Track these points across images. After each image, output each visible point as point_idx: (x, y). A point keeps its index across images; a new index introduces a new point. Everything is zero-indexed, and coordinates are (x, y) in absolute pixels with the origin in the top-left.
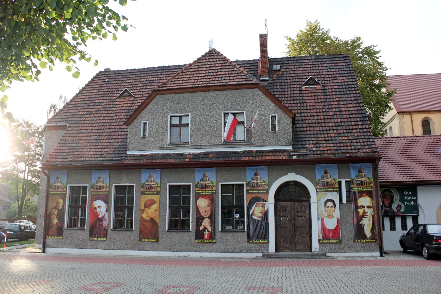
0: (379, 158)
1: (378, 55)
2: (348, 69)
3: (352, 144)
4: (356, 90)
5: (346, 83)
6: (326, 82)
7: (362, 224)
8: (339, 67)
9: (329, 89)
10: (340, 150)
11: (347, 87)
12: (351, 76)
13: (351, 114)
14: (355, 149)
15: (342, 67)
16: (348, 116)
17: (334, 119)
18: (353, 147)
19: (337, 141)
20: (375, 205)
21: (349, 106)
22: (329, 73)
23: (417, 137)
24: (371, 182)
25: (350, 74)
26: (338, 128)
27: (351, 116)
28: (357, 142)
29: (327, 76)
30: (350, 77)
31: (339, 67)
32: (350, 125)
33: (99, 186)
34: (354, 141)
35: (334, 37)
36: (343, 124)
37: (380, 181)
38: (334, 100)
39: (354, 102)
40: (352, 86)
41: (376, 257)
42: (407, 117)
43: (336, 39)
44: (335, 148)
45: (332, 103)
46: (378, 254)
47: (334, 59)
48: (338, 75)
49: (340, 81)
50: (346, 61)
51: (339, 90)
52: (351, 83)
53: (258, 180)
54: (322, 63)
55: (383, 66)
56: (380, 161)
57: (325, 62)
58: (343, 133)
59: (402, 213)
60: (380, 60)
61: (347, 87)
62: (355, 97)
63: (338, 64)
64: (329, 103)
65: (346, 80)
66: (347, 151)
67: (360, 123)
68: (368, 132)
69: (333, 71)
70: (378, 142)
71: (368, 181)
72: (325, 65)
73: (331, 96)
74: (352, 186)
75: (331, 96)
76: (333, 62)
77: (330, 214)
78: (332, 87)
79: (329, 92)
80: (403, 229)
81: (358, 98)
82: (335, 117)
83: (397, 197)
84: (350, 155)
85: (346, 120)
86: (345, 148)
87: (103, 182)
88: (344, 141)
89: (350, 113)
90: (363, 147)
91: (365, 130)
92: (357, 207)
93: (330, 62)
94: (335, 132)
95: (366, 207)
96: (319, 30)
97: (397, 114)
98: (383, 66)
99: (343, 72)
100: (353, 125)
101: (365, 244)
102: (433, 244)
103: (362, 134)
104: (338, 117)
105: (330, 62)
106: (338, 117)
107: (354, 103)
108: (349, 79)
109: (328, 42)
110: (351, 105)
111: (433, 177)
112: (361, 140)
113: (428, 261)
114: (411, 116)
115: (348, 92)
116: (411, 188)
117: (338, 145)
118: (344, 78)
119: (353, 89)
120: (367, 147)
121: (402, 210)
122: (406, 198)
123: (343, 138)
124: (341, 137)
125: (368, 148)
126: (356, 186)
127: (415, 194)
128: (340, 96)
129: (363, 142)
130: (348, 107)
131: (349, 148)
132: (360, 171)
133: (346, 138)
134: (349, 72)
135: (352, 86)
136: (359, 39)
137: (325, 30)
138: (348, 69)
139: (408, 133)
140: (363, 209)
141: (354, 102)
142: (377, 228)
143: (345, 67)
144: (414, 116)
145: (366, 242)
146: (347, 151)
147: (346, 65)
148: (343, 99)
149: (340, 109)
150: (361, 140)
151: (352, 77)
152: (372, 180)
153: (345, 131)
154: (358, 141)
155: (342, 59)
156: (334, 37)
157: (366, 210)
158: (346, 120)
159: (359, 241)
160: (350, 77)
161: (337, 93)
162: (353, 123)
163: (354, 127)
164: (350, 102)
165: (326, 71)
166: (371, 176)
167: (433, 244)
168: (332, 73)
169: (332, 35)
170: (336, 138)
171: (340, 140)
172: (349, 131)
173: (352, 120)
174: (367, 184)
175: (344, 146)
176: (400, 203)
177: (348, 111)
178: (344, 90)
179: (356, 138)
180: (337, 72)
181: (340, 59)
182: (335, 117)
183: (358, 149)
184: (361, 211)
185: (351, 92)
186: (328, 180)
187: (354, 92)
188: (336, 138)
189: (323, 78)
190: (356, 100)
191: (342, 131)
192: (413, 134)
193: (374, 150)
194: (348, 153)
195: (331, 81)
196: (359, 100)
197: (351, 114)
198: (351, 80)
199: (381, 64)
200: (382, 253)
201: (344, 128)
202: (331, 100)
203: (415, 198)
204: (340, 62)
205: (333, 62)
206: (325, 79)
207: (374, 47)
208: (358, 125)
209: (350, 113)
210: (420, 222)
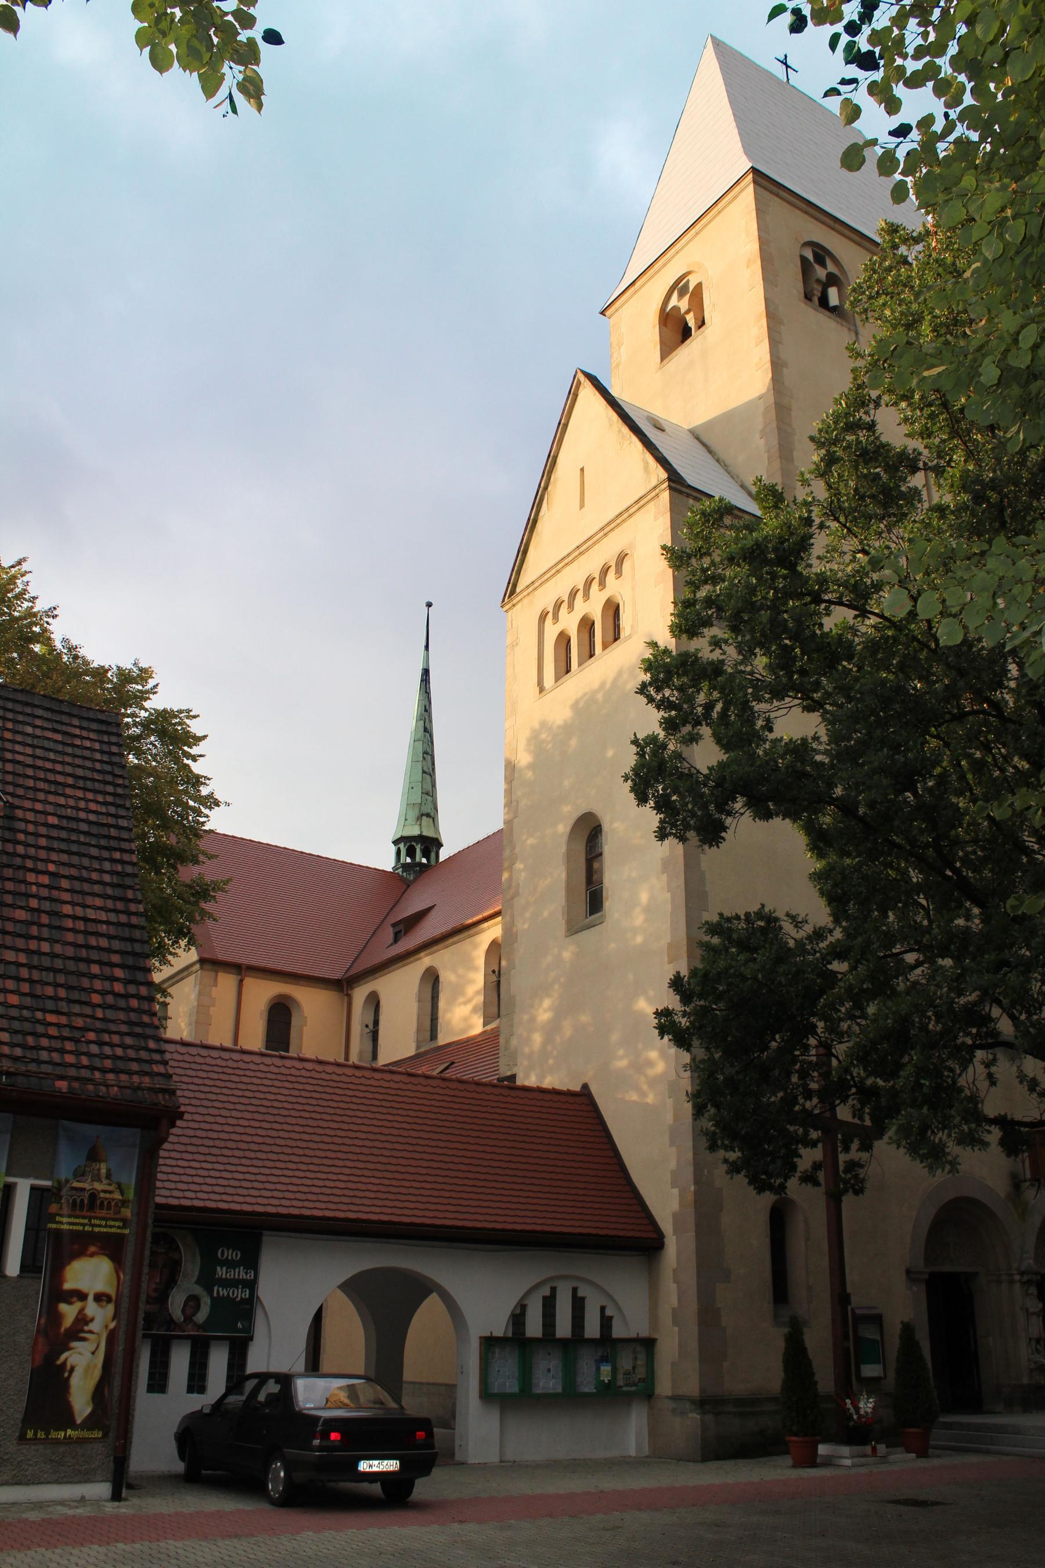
0: (174, 1115)
1: (194, 751)
2: (108, 768)
3: (83, 1048)
4: (123, 851)
5: (92, 817)
6: (20, 792)
7: (65, 1363)
8: (79, 752)
9: (27, 822)
10: (33, 1060)
11: (94, 830)
12: (114, 795)
13: (93, 934)
14: (92, 1068)
15: (87, 753)
16: (80, 939)
17: (28, 937)
18: (85, 1061)
19: (27, 1026)
20: (126, 1291)
21: (89, 900)
22: (40, 763)
23: (243, 1052)
24: (124, 1203)
25: (110, 789)
26: (36, 975)
27: (93, 941)
28: (101, 1044)
29: (30, 772)
30: (110, 799)
31: (79, 752)
32: (83, 975)
33: (87, 1195)
34: (92, 1036)
35: (65, 640)
36: (59, 964)
37: (158, 1200)
38: (41, 866)
39: (109, 891)
40: (113, 832)
41: (97, 1502)
42: (227, 982)
43: (70, 649)
44: (18, 1052)
45: (31, 877)
46: (102, 1489)
47: (64, 719)
48: (70, 781)
49: (71, 802)
50: (106, 738)
51: (64, 834)
52: (111, 821)
54: (20, 718)
55: (204, 791)
56: (174, 1125)
57: (29, 720)
58: (56, 999)
59: (200, 1327)
60: (197, 768)
61: (94, 830)
62: (118, 873)
63: (78, 742)
64: (20, 874)
65: (93, 806)
66: (59, 1071)
67: (119, 973)
68: (145, 1012)
69: (54, 761)
70: (176, 1056)
71: (117, 1196)
72: (29, 730)
73: (32, 851)
74: (54, 1208)
75: (32, 851)
76: (58, 727)
78: (41, 818)
79: (27, 833)
80: (191, 1389)
81: (128, 881)
82: (34, 931)
83: (191, 1267)
84: (70, 1087)
85: (70, 951)
86: (56, 1057)
88: (53, 1031)
89: (92, 928)
90: (121, 1065)
91: (134, 1003)
92: (58, 1295)
93: (46, 725)
94: (25, 988)
95: (91, 1298)
96: (20, 596)
97: (198, 966)
98: (204, 791)
99: (88, 774)
100: (95, 976)
101: (62, 1449)
102: (312, 1449)
103: (122, 1016)
104: (46, 933)
105: (46, 725)
106: (46, 933)
107: (109, 897)
108: (105, 804)
109: (37, 648)
110: (99, 902)
111: (373, 1209)
112: (116, 1039)
113: (283, 1510)
114: (241, 981)
115: (94, 852)
116: (240, 1236)
117: (30, 1041)
118: (90, 796)
119: (113, 843)
120: (135, 1066)
121: (201, 1316)
122: (221, 1272)
123: (51, 1018)
124: (44, 1011)
125: (136, 1073)
126: (65, 1211)
127: (252, 1261)
128: (64, 858)
129: (125, 1047)
130: (85, 906)
131: (70, 1059)
132: (93, 1156)
133: (64, 1020)
134: (109, 778)
135: (113, 832)
136: (144, 674)
137: (40, 606)
138: (108, 768)
139: (220, 1035)
140: (78, 1305)
141: (109, 891)
142: (117, 1382)
143: (98, 756)
144: (249, 982)
145: (68, 1440)
146: (59, 1071)
147: (102, 752)
148: (74, 872)
149: (56, 907)
150: (116, 1039)
151: (119, 801)
152: (131, 1194)
153: (62, 993)
154: (106, 1038)
155: (94, 726)
156: (65, 640)
157: (91, 1308)
158: (70, 951)
159: (41, 1435)
160: (110, 799)
161: (56, 845)
162: (95, 969)
163: (98, 985)
164: (97, 888)
165: (29, 751)
166: (130, 1179)
167: (312, 1449)
168: (49, 765)
169: (59, 631)
170: (26, 1013)
171: (38, 1021)
172: (76, 995)
173: (94, 955)
174: (109, 1208)
175: (50, 1050)
176: (198, 1290)
177: (86, 920)
178: (82, 838)
179: (99, 1025)
180: (69, 769)
181: (85, 724)
182: (34, 931)
183: (104, 1071)
184: (69, 1312)
185: (106, 854)
186: (98, 1186)
187: (117, 855)
188: (26, 1013)
189: (13, 773)
190: (118, 886)
191: (50, 991)
192: (236, 1041)
193: (160, 1083)
194: (62, 1078)
195: (41, 796)
196: (130, 887)
197: (93, 934)
198: (112, 810)
199: (197, 781)
200: (122, 1484)
201: (61, 979)
202: (29, 864)
203: (251, 1275)
204: (85, 734)
205: (58, 727)
206: (21, 781)
207: (188, 717)
208: (113, 979)
209: (92, 928)
210: (250, 1369)
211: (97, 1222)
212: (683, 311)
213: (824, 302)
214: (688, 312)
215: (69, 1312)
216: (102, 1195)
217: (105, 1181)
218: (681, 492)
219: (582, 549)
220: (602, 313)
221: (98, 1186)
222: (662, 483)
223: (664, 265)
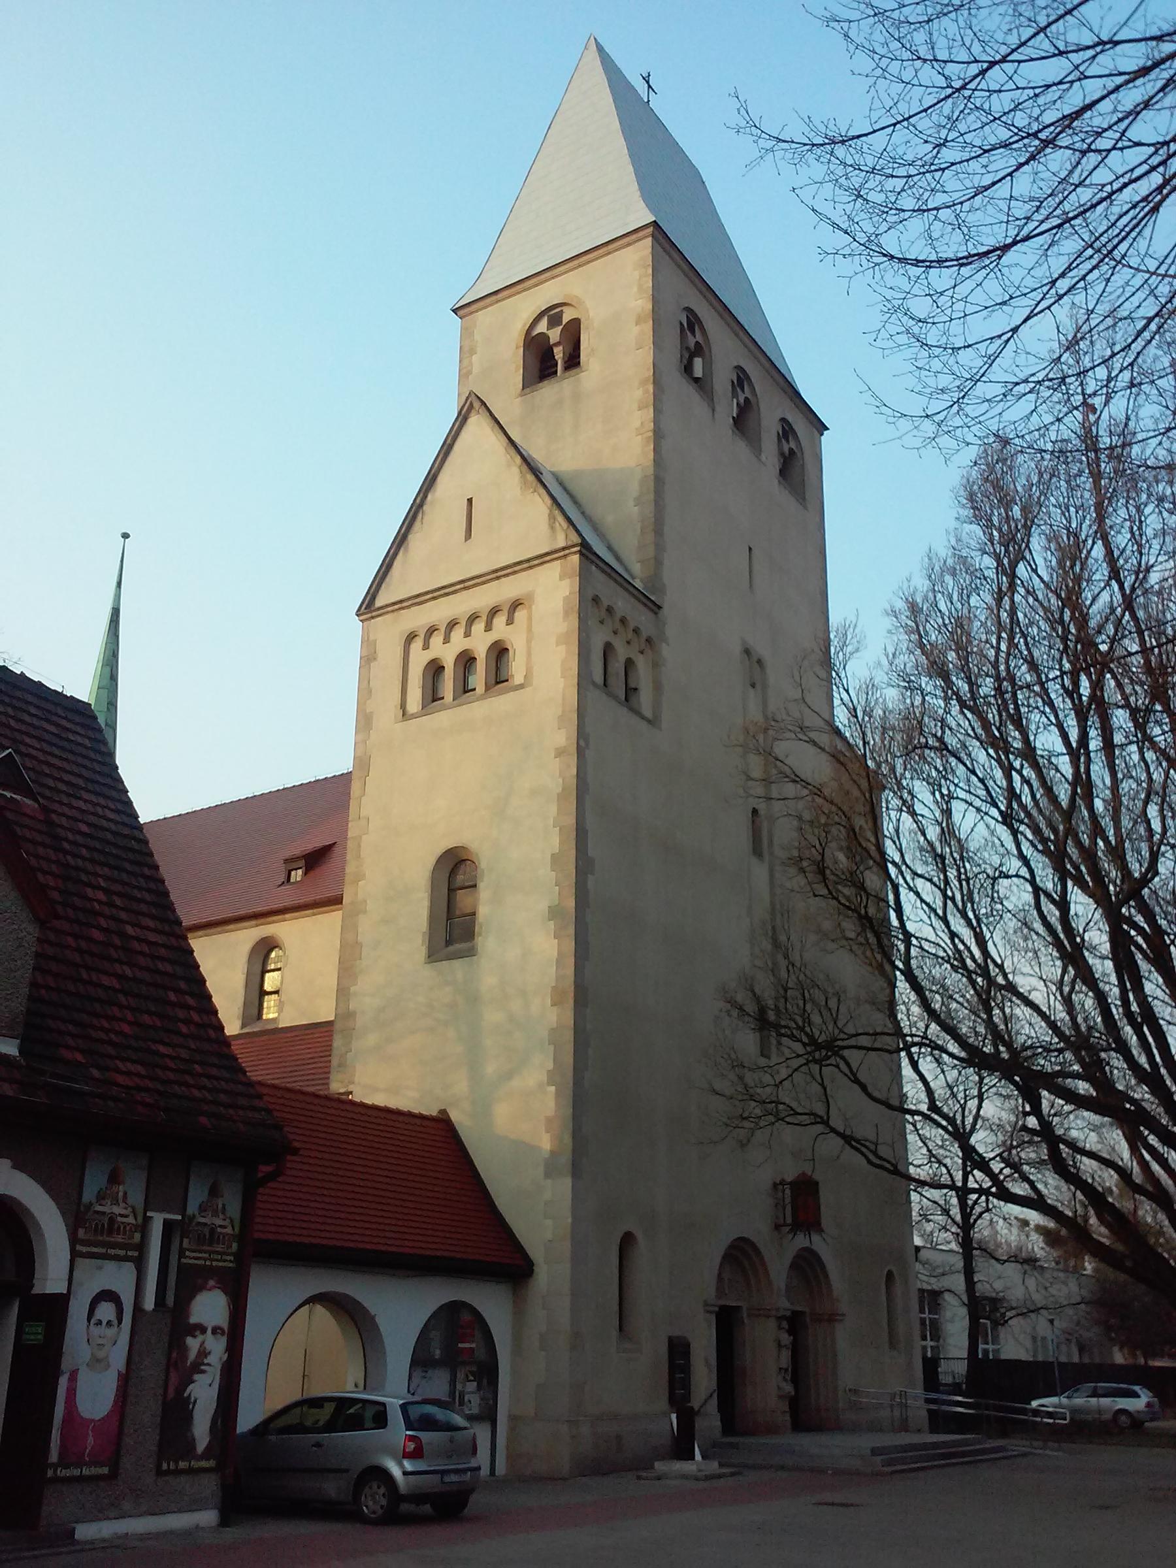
37: (256, 1235)
46: (208, 1517)
53: (215, 1214)
77: (101, 1354)
87: (124, 1201)
95: (209, 1331)
145: (191, 1471)
184: (193, 1344)
211: (216, 1257)
212: (552, 342)
213: (688, 369)
214: (557, 344)
215: (193, 1344)
216: (219, 1230)
217: (122, 1205)
218: (587, 558)
219: (467, 584)
220: (455, 311)
221: (117, 1210)
222: (574, 546)
223: (537, 285)
